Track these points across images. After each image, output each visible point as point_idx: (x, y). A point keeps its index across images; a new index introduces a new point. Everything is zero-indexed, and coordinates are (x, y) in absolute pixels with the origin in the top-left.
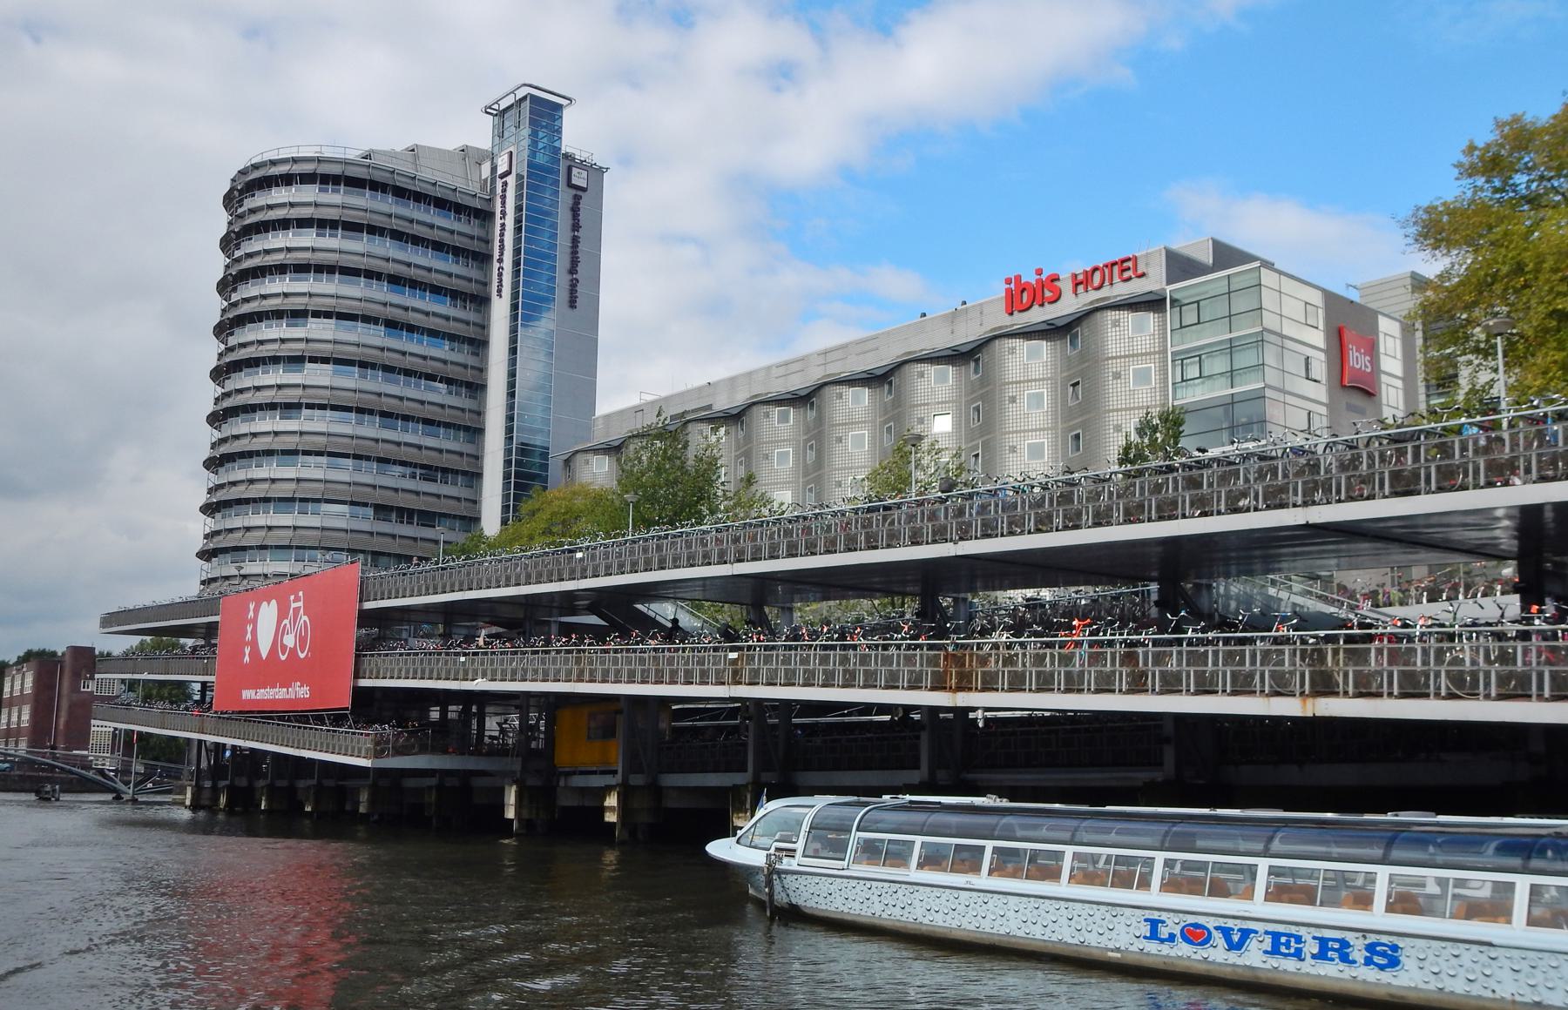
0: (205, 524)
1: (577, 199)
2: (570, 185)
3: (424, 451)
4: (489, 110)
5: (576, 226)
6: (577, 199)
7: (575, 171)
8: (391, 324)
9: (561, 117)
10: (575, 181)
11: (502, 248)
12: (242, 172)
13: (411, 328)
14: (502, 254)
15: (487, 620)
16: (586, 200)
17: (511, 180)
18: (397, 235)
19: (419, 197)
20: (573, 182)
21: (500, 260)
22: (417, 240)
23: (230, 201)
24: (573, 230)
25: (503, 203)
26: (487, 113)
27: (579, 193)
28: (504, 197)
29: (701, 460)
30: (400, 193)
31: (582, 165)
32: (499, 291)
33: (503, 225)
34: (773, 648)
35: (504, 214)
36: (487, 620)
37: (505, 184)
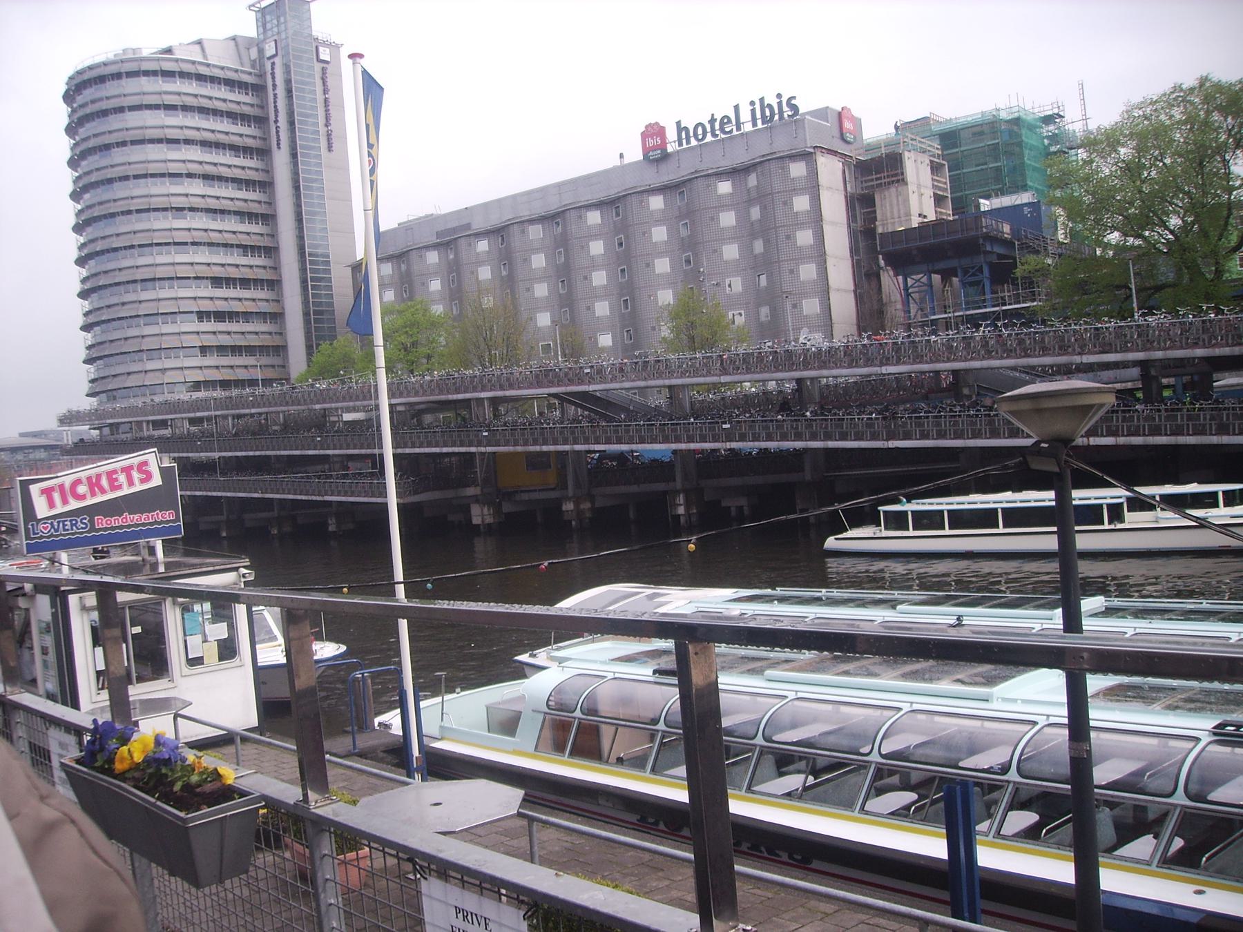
0: (89, 338)
1: (324, 70)
2: (319, 60)
3: (241, 268)
4: (252, 8)
5: (325, 91)
6: (324, 70)
7: (321, 49)
8: (206, 177)
9: (309, 10)
10: (322, 57)
11: (276, 111)
12: (79, 73)
13: (220, 178)
14: (276, 116)
15: (746, 616)
16: (330, 69)
17: (277, 60)
18: (203, 111)
19: (213, 80)
20: (274, 52)
21: (276, 121)
22: (216, 113)
23: (68, 97)
24: (325, 94)
25: (273, 78)
26: (250, 9)
27: (325, 65)
28: (273, 74)
29: (762, 360)
30: (200, 78)
31: (325, 44)
32: (278, 144)
33: (275, 95)
34: (630, 425)
35: (274, 86)
36: (746, 616)
37: (273, 64)
